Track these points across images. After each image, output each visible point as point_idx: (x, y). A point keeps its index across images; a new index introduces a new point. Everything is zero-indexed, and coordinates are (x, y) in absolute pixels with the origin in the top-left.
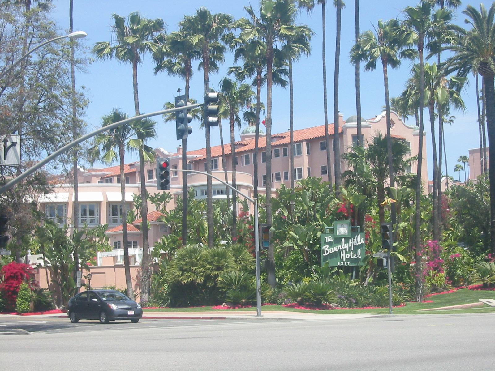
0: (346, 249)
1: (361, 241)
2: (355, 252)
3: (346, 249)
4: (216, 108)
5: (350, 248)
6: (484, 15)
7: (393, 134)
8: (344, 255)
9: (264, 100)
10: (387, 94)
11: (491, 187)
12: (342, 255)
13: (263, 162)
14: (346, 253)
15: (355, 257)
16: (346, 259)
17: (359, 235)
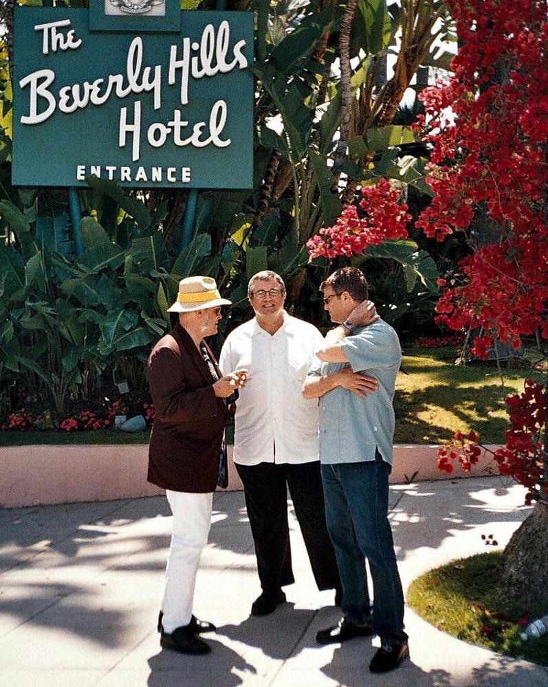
2: (197, 112)
5: (170, 91)
8: (136, 128)
12: (124, 128)
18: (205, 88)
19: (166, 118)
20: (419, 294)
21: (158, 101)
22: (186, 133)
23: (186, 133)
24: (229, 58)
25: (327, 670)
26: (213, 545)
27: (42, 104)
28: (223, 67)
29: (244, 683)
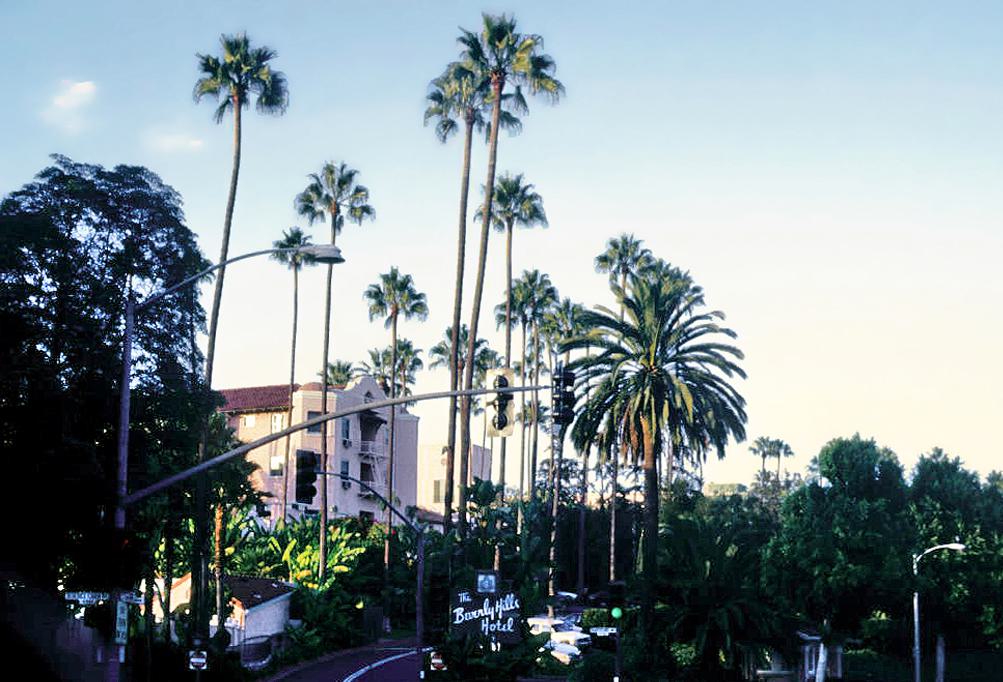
0: (489, 616)
1: (514, 605)
2: (504, 621)
3: (489, 616)
4: (118, 523)
5: (496, 615)
6: (502, 126)
7: (275, 626)
8: (487, 625)
9: (488, 440)
10: (493, 167)
11: (88, 591)
12: (483, 625)
13: (362, 513)
14: (491, 622)
15: (504, 629)
16: (489, 632)
17: (512, 595)
18: (507, 614)
19: (495, 622)
20: (708, 564)
21: (292, 483)
22: (501, 627)
23: (501, 627)
24: (514, 605)
25: (496, 353)
26: (917, 473)
27: (460, 618)
28: (512, 608)
29: (547, 230)
